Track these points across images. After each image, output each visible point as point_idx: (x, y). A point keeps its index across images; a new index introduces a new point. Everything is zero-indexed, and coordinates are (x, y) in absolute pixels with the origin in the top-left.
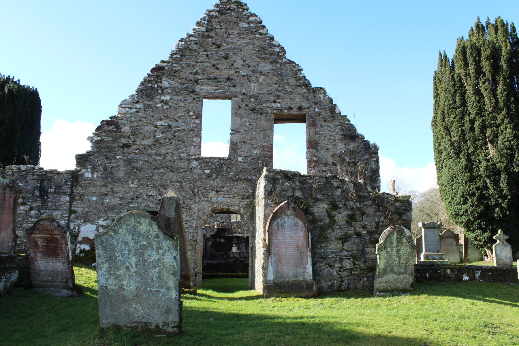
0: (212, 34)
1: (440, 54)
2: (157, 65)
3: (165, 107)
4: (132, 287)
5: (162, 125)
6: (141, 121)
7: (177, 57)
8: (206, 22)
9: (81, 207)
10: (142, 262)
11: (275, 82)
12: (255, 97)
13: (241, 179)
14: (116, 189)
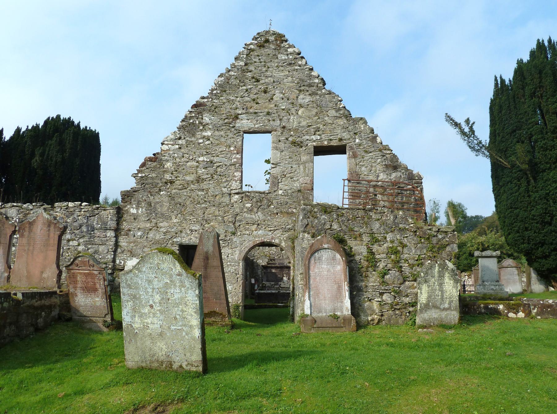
0: (251, 68)
1: (496, 78)
2: (197, 102)
3: (207, 142)
4: (156, 326)
5: (203, 161)
6: (183, 157)
7: (217, 93)
8: (245, 56)
9: (127, 242)
10: (165, 300)
11: (314, 113)
12: (296, 130)
13: (281, 212)
14: (161, 224)
